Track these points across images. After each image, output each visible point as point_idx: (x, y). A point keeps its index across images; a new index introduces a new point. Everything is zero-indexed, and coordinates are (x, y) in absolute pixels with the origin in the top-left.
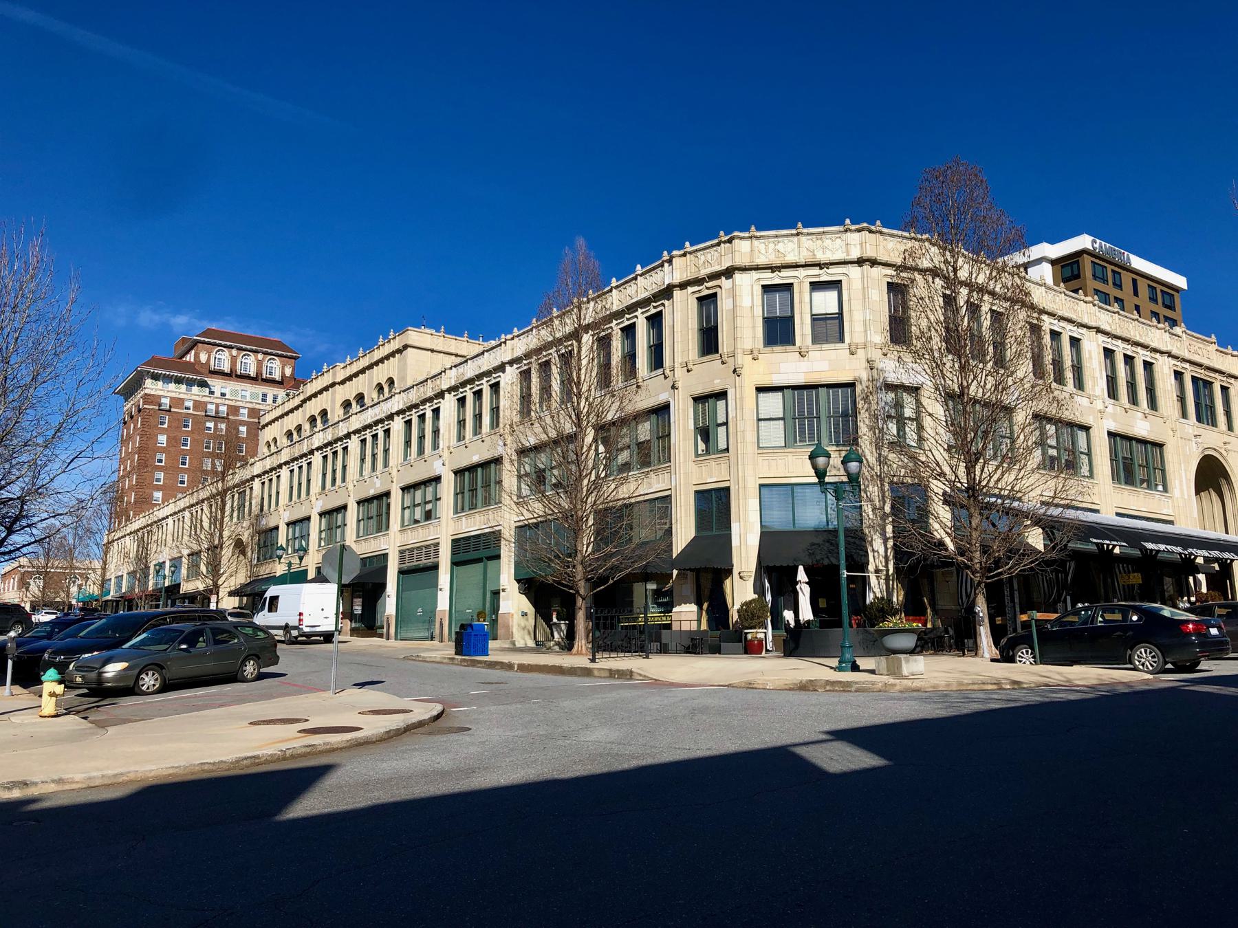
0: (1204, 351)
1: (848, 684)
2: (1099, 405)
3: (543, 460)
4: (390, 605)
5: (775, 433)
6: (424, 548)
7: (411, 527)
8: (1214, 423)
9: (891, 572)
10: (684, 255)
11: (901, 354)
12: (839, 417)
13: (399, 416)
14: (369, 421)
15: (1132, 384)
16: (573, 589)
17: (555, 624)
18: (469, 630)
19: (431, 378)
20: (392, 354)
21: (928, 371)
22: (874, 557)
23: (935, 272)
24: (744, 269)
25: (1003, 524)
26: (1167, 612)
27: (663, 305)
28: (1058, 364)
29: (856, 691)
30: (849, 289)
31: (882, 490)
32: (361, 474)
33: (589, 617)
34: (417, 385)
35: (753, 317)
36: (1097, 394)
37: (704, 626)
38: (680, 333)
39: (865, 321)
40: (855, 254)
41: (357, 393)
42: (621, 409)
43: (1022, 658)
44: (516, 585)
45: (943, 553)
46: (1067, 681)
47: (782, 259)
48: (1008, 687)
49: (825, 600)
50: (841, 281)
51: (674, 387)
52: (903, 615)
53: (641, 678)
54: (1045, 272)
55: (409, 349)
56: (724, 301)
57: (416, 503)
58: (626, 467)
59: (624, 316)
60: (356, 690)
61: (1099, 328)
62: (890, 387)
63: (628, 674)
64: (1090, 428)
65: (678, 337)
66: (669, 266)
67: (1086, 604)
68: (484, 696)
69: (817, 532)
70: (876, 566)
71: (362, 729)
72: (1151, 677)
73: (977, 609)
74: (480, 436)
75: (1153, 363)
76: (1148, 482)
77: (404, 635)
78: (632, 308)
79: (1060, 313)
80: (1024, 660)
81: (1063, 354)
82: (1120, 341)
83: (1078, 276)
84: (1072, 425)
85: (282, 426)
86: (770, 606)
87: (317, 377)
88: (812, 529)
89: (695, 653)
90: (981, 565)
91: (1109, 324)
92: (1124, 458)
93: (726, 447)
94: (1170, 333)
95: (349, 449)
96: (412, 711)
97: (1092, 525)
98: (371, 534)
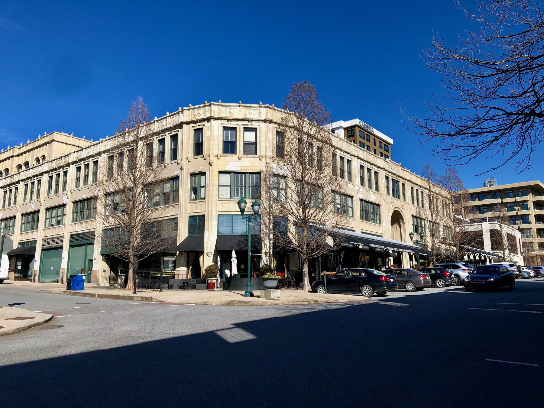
1: (248, 302)
2: (357, 188)
3: (117, 198)
4: (36, 265)
5: (226, 192)
6: (55, 238)
7: (49, 228)
8: (399, 198)
9: (271, 253)
10: (189, 110)
11: (279, 162)
12: (254, 187)
13: (46, 174)
14: (30, 175)
15: (370, 180)
16: (127, 260)
17: (119, 275)
18: (74, 278)
19: (64, 157)
20: (45, 144)
21: (290, 169)
22: (265, 247)
23: (295, 128)
25: (316, 234)
26: (376, 272)
27: (178, 131)
28: (342, 170)
29: (251, 305)
30: (260, 132)
31: (270, 220)
32: (25, 201)
33: (134, 273)
34: (56, 159)
35: (218, 140)
37: (190, 277)
38: (185, 144)
39: (266, 147)
40: (263, 117)
41: (5, 168)
42: (154, 177)
43: (320, 290)
44: (101, 257)
45: (291, 246)
46: (337, 301)
47: (232, 116)
48: (313, 303)
49: (243, 265)
50: (257, 128)
51: (181, 169)
52: (275, 272)
53: (156, 301)
54: (341, 133)
55: (54, 142)
56: (206, 132)
57: (53, 216)
58: (157, 204)
59: (197, 123)
60: (9, 308)
61: (358, 157)
62: (275, 175)
63: (151, 299)
64: (353, 197)
65: (184, 146)
66: (182, 114)
67: (347, 269)
68: (77, 309)
69: (242, 236)
70: (265, 251)
71: (4, 327)
72: (368, 298)
73: (304, 270)
74: (87, 185)
75: (378, 172)
76: (374, 220)
77: (43, 280)
78: (163, 131)
79: (344, 149)
80: (321, 291)
81: (344, 166)
82: (366, 163)
83: (353, 135)
84: (347, 195)
85: (33, 155)
86: (219, 268)
87: (4, 152)
88: (240, 235)
89: (184, 289)
90: (306, 251)
91: (363, 156)
92: (365, 210)
93: (204, 197)
94: (385, 161)
95: (18, 188)
96: (35, 318)
97: (351, 236)
98: (28, 231)
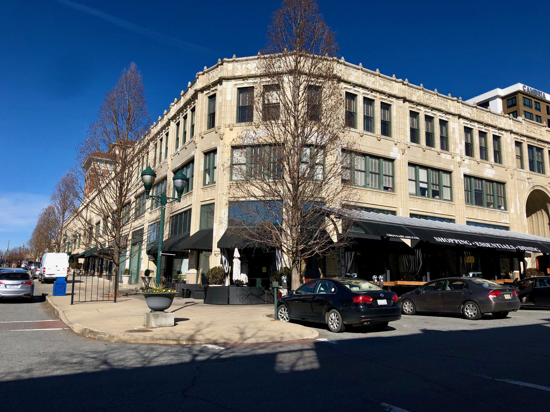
0: (538, 131)
24: (228, 79)
29: (98, 340)
36: (457, 153)
75: (500, 137)
82: (476, 123)
83: (515, 105)
91: (470, 114)
97: (401, 226)
